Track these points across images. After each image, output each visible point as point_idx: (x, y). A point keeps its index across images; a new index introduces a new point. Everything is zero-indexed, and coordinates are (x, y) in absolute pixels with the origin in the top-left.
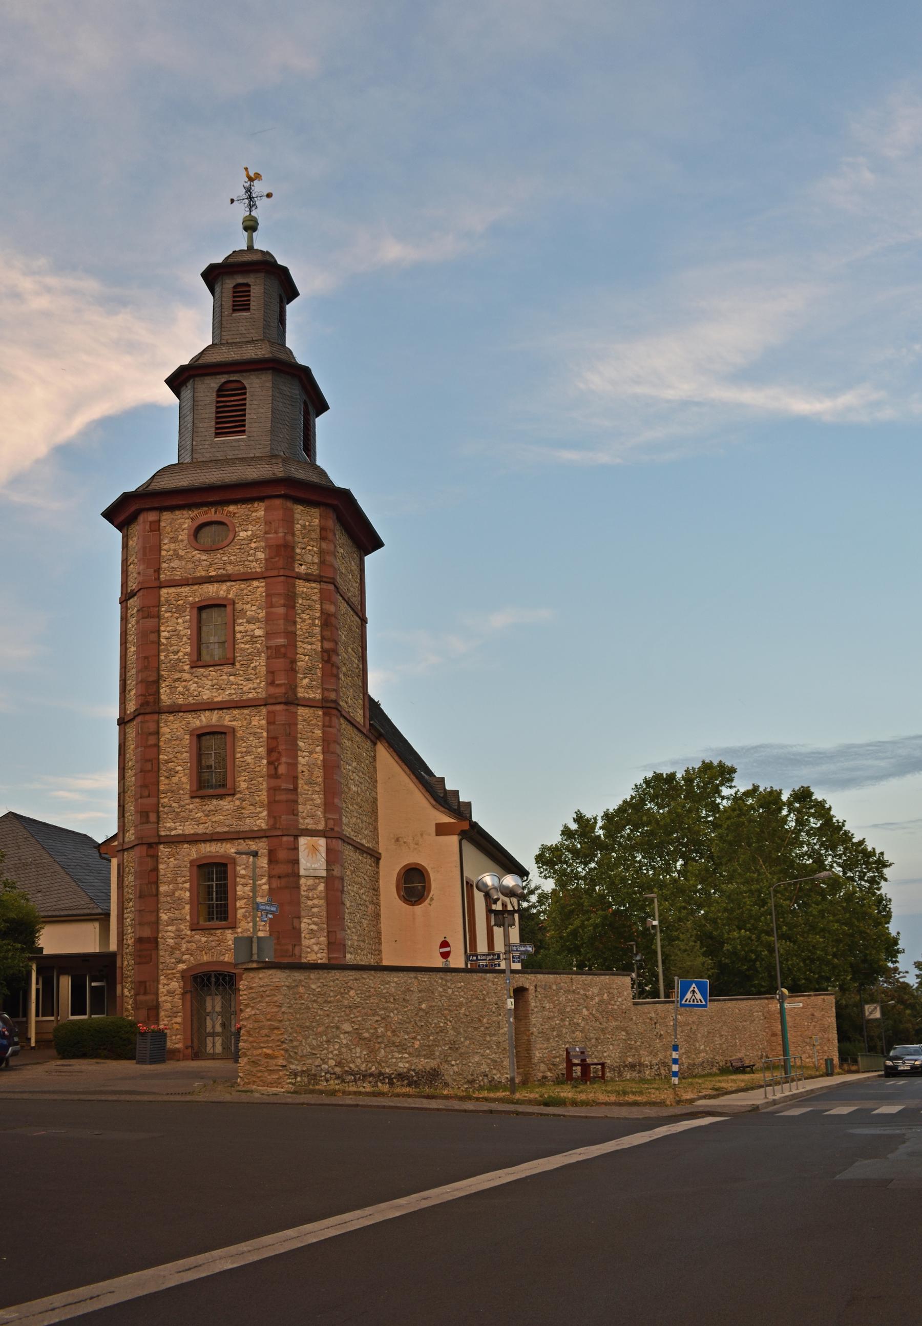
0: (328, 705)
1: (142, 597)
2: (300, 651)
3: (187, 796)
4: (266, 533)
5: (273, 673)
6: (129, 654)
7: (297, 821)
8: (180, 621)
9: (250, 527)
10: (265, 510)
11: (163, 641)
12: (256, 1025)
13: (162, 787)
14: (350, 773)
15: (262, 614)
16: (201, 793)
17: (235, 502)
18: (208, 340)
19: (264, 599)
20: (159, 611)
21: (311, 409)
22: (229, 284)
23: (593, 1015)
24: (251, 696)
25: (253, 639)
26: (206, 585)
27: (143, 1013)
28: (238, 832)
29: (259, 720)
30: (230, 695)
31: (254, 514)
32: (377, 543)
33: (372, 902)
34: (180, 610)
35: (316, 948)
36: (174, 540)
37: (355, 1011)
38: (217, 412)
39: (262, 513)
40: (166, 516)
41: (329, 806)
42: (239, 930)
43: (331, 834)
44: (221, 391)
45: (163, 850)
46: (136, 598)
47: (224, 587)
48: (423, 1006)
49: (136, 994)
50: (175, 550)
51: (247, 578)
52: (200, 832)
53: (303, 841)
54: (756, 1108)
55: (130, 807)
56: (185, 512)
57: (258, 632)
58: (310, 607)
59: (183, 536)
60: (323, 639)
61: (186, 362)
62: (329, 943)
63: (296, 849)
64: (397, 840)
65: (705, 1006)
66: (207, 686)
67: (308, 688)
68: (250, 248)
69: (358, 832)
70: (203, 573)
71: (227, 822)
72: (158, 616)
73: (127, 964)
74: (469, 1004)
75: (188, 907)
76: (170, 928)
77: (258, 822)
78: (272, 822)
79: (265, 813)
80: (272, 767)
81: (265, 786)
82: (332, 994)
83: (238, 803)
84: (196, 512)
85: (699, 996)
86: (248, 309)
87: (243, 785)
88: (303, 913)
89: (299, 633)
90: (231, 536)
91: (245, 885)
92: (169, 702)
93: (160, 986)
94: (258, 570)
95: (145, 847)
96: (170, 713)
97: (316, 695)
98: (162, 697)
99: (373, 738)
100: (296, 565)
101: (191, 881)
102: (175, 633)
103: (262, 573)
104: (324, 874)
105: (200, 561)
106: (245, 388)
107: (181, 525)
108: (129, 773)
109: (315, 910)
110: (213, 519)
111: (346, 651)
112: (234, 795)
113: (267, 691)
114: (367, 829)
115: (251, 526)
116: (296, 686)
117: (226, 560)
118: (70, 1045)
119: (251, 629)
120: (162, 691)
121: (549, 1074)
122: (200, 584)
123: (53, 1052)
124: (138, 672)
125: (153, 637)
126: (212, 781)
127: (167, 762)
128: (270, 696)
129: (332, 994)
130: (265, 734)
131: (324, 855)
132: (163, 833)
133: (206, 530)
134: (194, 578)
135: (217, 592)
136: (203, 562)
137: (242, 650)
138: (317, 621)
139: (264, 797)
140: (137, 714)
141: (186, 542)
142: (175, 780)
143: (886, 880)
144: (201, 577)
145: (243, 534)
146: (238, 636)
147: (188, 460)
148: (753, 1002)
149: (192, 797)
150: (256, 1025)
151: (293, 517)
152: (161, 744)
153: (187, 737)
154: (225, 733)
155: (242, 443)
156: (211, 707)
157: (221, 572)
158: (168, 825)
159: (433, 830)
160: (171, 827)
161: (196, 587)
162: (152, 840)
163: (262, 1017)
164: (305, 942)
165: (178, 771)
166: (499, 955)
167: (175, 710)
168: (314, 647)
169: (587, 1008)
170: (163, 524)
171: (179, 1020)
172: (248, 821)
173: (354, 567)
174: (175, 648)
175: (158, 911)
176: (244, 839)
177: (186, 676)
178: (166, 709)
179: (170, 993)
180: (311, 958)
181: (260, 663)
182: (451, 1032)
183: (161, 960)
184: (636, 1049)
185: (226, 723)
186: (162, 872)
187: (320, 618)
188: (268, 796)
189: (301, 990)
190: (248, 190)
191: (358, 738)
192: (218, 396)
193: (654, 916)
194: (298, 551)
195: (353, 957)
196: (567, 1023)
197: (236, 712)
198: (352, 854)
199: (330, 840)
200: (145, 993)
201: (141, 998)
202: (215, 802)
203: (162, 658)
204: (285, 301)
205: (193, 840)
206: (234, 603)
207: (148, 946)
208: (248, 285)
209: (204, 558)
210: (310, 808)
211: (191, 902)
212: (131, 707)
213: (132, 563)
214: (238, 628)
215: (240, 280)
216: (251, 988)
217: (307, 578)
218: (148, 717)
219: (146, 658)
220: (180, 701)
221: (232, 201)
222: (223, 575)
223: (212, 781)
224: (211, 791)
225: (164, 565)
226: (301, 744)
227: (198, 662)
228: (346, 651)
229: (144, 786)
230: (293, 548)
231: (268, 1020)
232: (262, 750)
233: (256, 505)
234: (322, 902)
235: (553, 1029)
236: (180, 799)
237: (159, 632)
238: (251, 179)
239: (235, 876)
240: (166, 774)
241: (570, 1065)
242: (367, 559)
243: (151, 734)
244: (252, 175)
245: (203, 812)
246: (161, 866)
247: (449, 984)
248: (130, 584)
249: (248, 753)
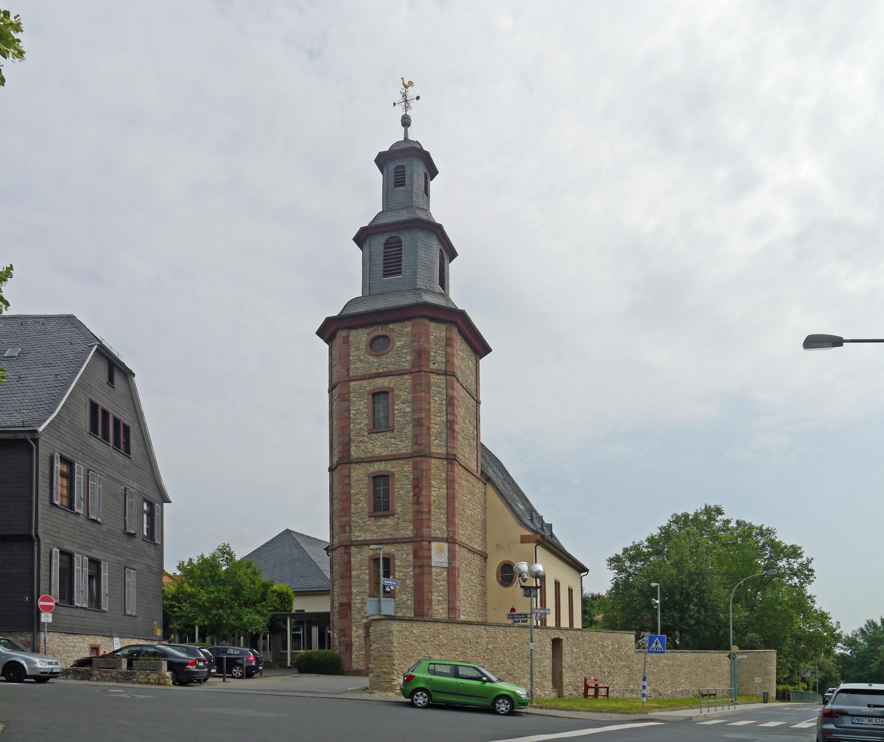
2: (433, 422)
9: (403, 339)
10: (412, 326)
13: (352, 511)
15: (410, 398)
16: (375, 514)
17: (393, 322)
18: (378, 207)
25: (405, 414)
26: (377, 379)
27: (343, 648)
29: (408, 467)
32: (487, 350)
35: (441, 611)
36: (357, 349)
38: (385, 260)
39: (409, 329)
40: (353, 333)
43: (451, 540)
44: (387, 245)
45: (354, 550)
47: (388, 379)
48: (490, 647)
49: (340, 637)
51: (400, 374)
54: (691, 718)
55: (336, 523)
58: (440, 393)
59: (363, 346)
62: (449, 608)
63: (430, 549)
64: (498, 546)
65: (663, 652)
66: (378, 445)
67: (437, 446)
69: (472, 540)
70: (375, 371)
72: (348, 400)
73: (335, 618)
75: (367, 585)
81: (411, 510)
85: (660, 646)
86: (404, 185)
87: (399, 509)
88: (434, 590)
91: (400, 572)
92: (356, 456)
95: (343, 548)
101: (369, 569)
102: (358, 411)
104: (447, 565)
105: (373, 362)
106: (401, 242)
108: (335, 502)
109: (441, 588)
111: (465, 422)
115: (401, 335)
117: (387, 362)
118: (307, 666)
119: (402, 408)
123: (296, 671)
125: (346, 414)
126: (381, 506)
128: (415, 451)
136: (374, 364)
139: (410, 516)
142: (360, 506)
143: (524, 540)
145: (398, 344)
146: (396, 412)
147: (367, 294)
151: (428, 330)
156: (379, 459)
157: (385, 369)
159: (519, 539)
160: (358, 535)
163: (382, 649)
164: (435, 608)
165: (362, 501)
167: (360, 461)
170: (351, 338)
171: (363, 652)
172: (402, 532)
173: (472, 365)
174: (359, 421)
177: (366, 439)
179: (358, 636)
180: (438, 617)
181: (409, 430)
183: (353, 616)
185: (389, 469)
186: (353, 563)
189: (407, 633)
190: (405, 95)
191: (472, 479)
192: (385, 248)
194: (432, 354)
200: (344, 636)
201: (342, 639)
202: (383, 520)
204: (429, 178)
205: (367, 543)
206: (393, 391)
207: (346, 607)
208: (403, 167)
210: (437, 525)
211: (370, 582)
212: (335, 460)
214: (396, 407)
218: (344, 466)
219: (342, 427)
220: (362, 455)
221: (395, 104)
223: (381, 506)
224: (381, 513)
225: (352, 366)
226: (433, 482)
228: (465, 422)
229: (343, 510)
230: (429, 352)
234: (445, 583)
235: (578, 665)
237: (349, 411)
238: (406, 87)
239: (395, 566)
241: (587, 687)
243: (346, 477)
246: (353, 560)
249: (402, 488)
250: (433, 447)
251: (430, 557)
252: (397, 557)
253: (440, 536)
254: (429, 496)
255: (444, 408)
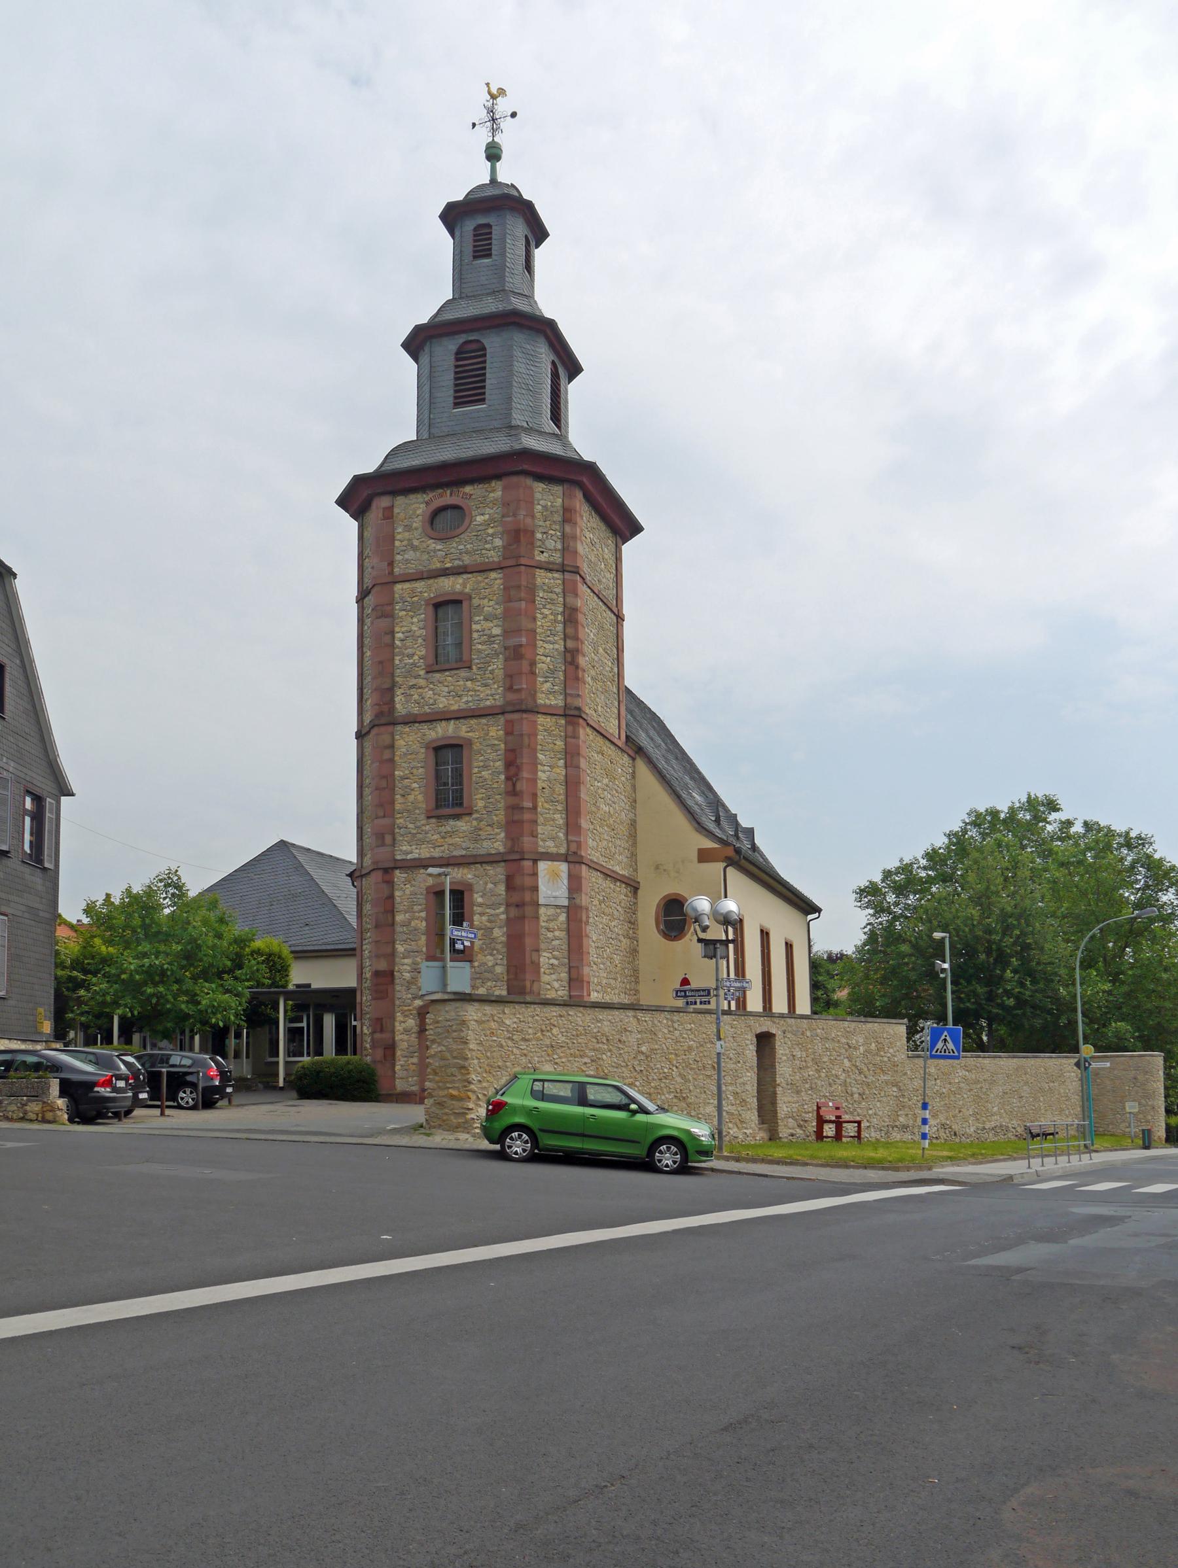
0: (572, 712)
1: (375, 592)
3: (423, 816)
4: (503, 516)
5: (511, 676)
6: (366, 659)
7: (536, 843)
8: (415, 620)
9: (488, 510)
10: (505, 489)
11: (398, 643)
12: (442, 1063)
13: (398, 807)
14: (600, 791)
15: (500, 610)
17: (471, 481)
19: (501, 592)
20: (393, 609)
21: (561, 371)
22: (469, 226)
23: (856, 1067)
24: (488, 703)
27: (379, 1053)
28: (475, 856)
29: (495, 731)
30: (468, 702)
31: (492, 495)
33: (627, 936)
34: (414, 608)
35: (556, 985)
36: (408, 528)
37: (559, 1051)
38: (456, 379)
39: (499, 494)
40: (400, 501)
41: (572, 825)
42: (476, 964)
43: (573, 858)
44: (459, 354)
45: (399, 876)
46: (370, 597)
47: (460, 580)
48: (644, 1049)
50: (409, 540)
51: (483, 570)
52: (437, 855)
53: (543, 866)
56: (419, 496)
57: (497, 631)
58: (552, 602)
60: (565, 637)
61: (424, 319)
62: (570, 980)
64: (657, 868)
65: (957, 1058)
66: (443, 694)
67: (548, 694)
68: (493, 181)
69: (611, 857)
70: (439, 565)
71: (464, 845)
73: (365, 999)
74: (701, 1049)
75: (424, 938)
76: (406, 961)
77: (496, 845)
78: (509, 844)
79: (503, 835)
80: (510, 783)
81: (501, 805)
82: (530, 1031)
83: (475, 823)
84: (431, 495)
85: (951, 1046)
87: (481, 804)
88: (542, 946)
89: (538, 630)
90: (467, 522)
91: (482, 914)
93: (397, 1024)
94: (496, 559)
95: (379, 874)
96: (405, 723)
97: (557, 701)
98: (398, 706)
99: (631, 752)
100: (536, 553)
101: (427, 910)
103: (499, 562)
105: (435, 551)
106: (484, 349)
107: (415, 510)
108: (367, 791)
110: (449, 503)
111: (596, 652)
112: (470, 814)
113: (504, 697)
114: (621, 854)
115: (485, 504)
116: (535, 692)
117: (461, 549)
118: (312, 1086)
119: (485, 628)
120: (397, 699)
121: (799, 1131)
122: (435, 577)
123: (294, 1094)
124: (373, 679)
125: (387, 639)
126: (449, 799)
127: (403, 778)
128: (508, 703)
129: (530, 1031)
130: (503, 746)
131: (566, 882)
132: (398, 857)
133: (442, 515)
134: (430, 571)
135: (453, 586)
136: (438, 553)
137: (479, 651)
138: (560, 617)
140: (373, 726)
141: (420, 530)
142: (411, 798)
144: (437, 570)
145: (479, 519)
146: (475, 635)
147: (426, 436)
148: (1064, 1061)
149: (428, 818)
150: (442, 1063)
151: (532, 496)
152: (396, 758)
153: (423, 750)
154: (461, 746)
155: (481, 414)
157: (457, 563)
158: (404, 848)
159: (694, 856)
160: (407, 850)
161: (431, 581)
162: (387, 865)
163: (448, 1055)
164: (545, 978)
166: (709, 991)
167: (412, 720)
168: (557, 646)
169: (850, 1059)
170: (396, 510)
172: (485, 844)
173: (608, 554)
174: (410, 651)
175: (394, 942)
176: (481, 863)
177: (422, 682)
178: (400, 720)
179: (407, 1031)
180: (551, 995)
181: (497, 665)
182: (679, 1080)
183: (398, 995)
184: (910, 1108)
186: (398, 900)
187: (563, 613)
188: (506, 816)
189: (493, 1025)
190: (491, 111)
191: (611, 751)
192: (457, 360)
193: (944, 956)
194: (539, 536)
195: (600, 996)
196: (823, 1075)
197: (473, 722)
198: (600, 881)
199: (572, 866)
200: (382, 1031)
201: (377, 1036)
202: (452, 822)
203: (397, 662)
204: (533, 244)
206: (470, 598)
207: (385, 979)
208: (489, 226)
209: (439, 547)
210: (549, 831)
212: (368, 719)
213: (368, 557)
214: (474, 627)
215: (482, 220)
216: (438, 1022)
217: (548, 568)
218: (382, 729)
219: (381, 662)
220: (416, 710)
221: (474, 125)
222: (459, 567)
223: (449, 799)
225: (398, 557)
226: (540, 756)
227: (437, 664)
228: (596, 652)
229: (381, 805)
230: (533, 532)
231: (455, 1058)
232: (499, 764)
233: (493, 484)
234: (563, 934)
235: (805, 1081)
236: (416, 820)
237: (392, 633)
238: (493, 97)
240: (402, 792)
241: (821, 1121)
242: (626, 548)
244: (494, 91)
245: (439, 833)
246: (397, 893)
247: (676, 1025)
248: (366, 580)
249: (486, 767)
250: (539, 695)
251: (535, 889)
252: (476, 888)
253: (554, 850)
254: (534, 781)
255: (560, 627)
